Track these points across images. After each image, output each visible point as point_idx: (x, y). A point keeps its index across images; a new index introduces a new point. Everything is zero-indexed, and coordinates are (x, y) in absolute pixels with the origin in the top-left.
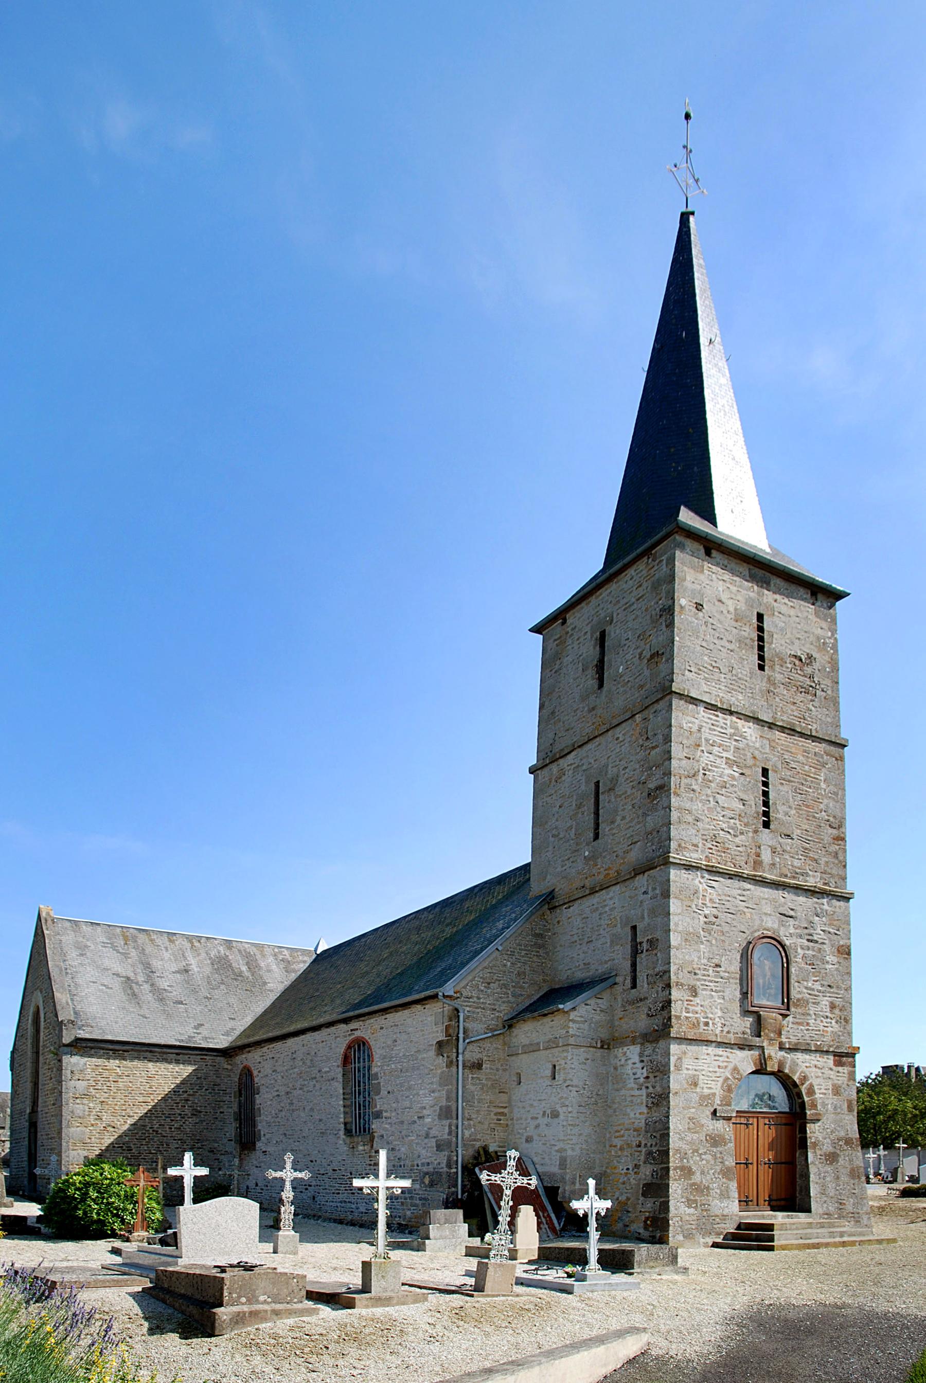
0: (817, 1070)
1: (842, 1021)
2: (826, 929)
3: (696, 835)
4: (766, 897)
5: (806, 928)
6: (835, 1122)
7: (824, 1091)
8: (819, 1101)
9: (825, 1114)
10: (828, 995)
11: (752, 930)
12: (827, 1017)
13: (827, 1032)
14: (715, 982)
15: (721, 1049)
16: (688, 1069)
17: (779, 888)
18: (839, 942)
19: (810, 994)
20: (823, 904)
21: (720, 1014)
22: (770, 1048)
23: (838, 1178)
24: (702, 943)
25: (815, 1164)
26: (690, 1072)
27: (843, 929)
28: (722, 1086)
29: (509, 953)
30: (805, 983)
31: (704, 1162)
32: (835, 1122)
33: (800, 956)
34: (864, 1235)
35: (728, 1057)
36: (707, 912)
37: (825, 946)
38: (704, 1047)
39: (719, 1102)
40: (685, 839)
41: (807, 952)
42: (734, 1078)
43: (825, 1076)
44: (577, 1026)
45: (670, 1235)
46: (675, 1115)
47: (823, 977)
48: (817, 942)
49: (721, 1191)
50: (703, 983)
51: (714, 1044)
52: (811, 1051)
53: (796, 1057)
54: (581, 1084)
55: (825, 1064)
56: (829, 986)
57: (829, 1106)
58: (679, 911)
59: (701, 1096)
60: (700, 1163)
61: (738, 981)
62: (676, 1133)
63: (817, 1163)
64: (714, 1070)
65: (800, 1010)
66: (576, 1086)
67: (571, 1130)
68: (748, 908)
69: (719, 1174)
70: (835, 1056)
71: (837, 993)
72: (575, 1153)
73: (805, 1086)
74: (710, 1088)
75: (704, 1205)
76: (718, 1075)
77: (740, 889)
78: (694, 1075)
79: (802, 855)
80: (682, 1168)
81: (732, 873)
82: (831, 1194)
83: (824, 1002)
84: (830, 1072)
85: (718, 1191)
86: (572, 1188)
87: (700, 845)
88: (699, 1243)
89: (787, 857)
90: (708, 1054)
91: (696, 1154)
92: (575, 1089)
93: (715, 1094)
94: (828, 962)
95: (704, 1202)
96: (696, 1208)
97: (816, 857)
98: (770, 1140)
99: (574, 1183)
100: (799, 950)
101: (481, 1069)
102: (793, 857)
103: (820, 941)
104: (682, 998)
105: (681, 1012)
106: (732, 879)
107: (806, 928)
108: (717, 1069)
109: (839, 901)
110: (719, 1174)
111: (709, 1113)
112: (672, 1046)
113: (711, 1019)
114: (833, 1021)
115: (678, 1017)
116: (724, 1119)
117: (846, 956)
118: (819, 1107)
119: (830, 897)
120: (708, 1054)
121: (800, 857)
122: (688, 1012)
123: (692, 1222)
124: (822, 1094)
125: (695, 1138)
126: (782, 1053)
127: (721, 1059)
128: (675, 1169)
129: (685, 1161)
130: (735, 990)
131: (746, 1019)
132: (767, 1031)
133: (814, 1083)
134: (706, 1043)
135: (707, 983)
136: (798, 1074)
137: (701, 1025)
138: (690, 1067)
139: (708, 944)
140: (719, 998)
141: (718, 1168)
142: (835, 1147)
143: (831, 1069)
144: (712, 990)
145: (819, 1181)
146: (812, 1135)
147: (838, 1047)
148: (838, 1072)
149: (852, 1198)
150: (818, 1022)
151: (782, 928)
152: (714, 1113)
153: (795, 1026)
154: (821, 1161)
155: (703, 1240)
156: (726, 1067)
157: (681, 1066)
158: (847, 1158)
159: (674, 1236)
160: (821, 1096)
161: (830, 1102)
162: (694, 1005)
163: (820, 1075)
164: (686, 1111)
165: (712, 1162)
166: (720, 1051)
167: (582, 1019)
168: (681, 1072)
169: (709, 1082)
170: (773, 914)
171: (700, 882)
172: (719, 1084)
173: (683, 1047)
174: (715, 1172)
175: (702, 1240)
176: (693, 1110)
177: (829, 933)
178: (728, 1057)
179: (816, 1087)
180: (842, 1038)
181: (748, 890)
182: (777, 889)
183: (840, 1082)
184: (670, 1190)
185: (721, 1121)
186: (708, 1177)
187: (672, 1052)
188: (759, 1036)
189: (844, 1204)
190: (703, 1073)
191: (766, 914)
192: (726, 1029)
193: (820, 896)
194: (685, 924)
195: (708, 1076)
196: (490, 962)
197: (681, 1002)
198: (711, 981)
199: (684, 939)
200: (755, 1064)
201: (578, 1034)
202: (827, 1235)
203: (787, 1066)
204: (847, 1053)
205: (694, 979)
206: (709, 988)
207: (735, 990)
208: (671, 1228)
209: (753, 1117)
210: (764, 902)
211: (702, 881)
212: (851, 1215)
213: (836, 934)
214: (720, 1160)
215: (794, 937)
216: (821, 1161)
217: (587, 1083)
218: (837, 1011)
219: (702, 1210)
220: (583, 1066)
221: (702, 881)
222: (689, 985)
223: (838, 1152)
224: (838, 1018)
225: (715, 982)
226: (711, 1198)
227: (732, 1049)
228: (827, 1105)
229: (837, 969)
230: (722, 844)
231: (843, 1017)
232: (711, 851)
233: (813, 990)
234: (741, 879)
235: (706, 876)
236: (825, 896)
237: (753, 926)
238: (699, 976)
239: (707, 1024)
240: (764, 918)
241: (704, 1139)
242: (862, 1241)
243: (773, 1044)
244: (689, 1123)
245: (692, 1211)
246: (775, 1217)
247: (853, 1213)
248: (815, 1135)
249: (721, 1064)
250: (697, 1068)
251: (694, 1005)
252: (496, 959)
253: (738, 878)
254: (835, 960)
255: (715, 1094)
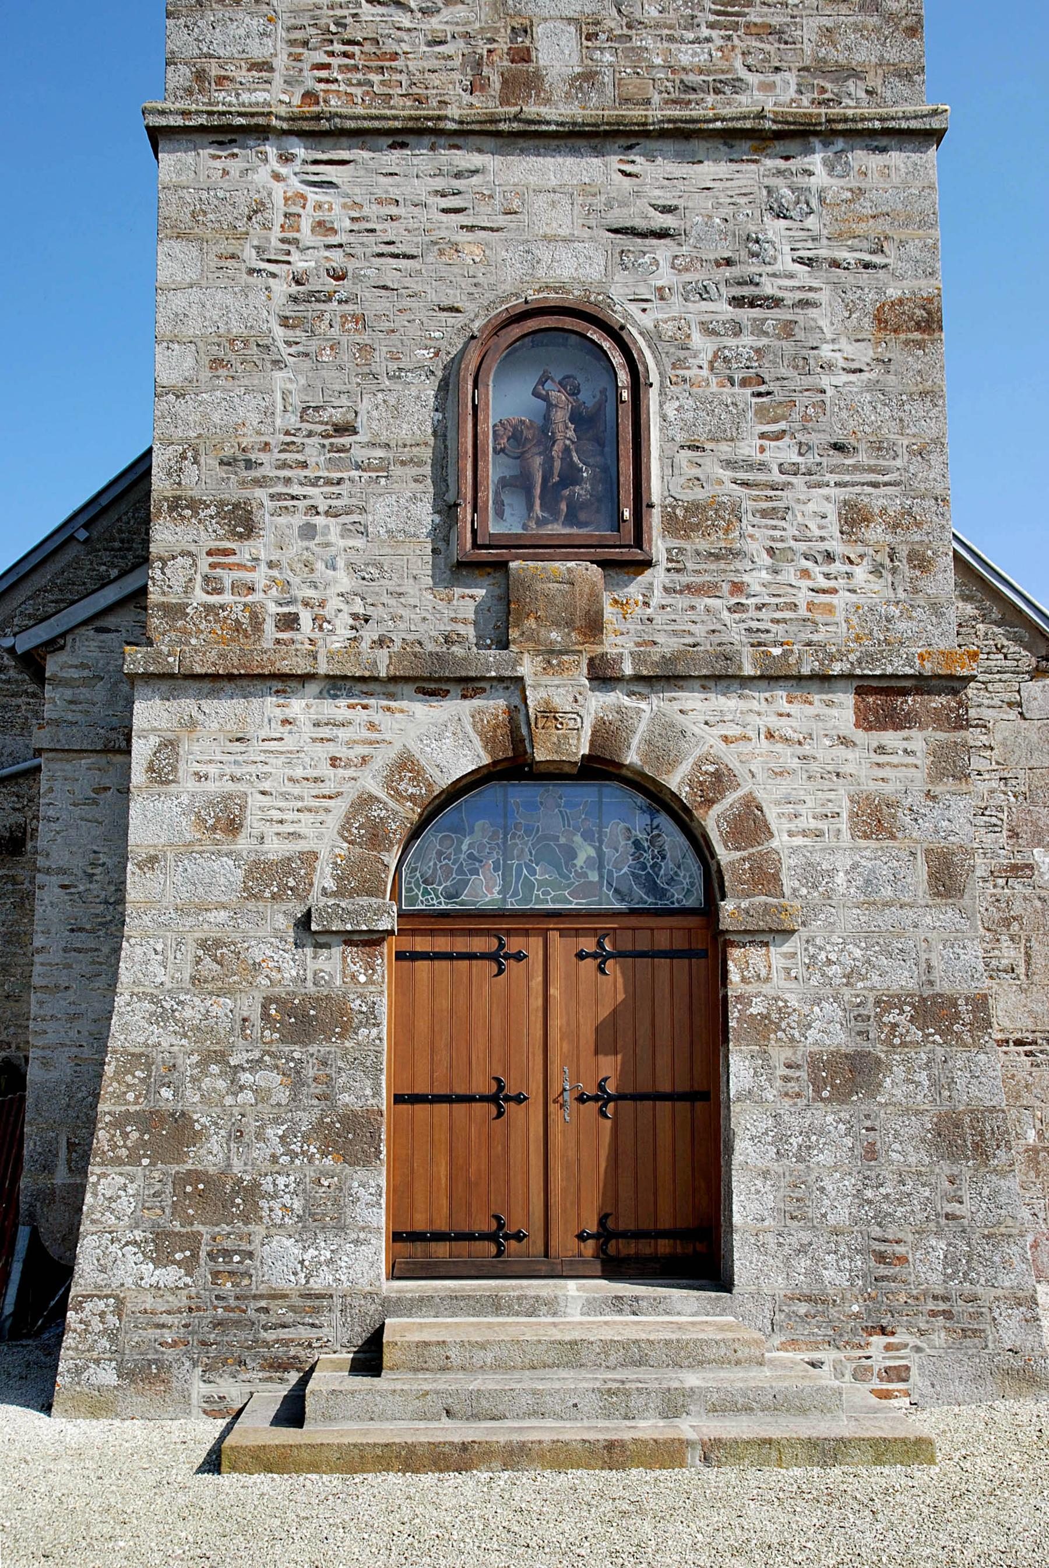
0: (779, 747)
1: (904, 566)
2: (823, 253)
3: (264, 34)
4: (554, 182)
5: (729, 262)
6: (867, 936)
7: (813, 824)
8: (788, 862)
9: (815, 910)
10: (832, 478)
11: (490, 296)
12: (829, 557)
13: (830, 609)
14: (329, 482)
15: (343, 702)
16: (199, 777)
17: (608, 145)
18: (880, 291)
19: (745, 484)
20: (811, 174)
21: (344, 581)
22: (546, 680)
23: (871, 1153)
24: (278, 364)
25: (762, 1101)
26: (211, 787)
27: (902, 243)
28: (345, 827)
29: (117, 545)
30: (724, 447)
31: (247, 1097)
32: (867, 936)
33: (704, 359)
34: (803, 1411)
35: (372, 726)
36: (300, 263)
37: (812, 312)
38: (271, 700)
39: (330, 885)
40: (221, 52)
41: (731, 342)
42: (398, 796)
43: (814, 767)
44: (68, 693)
45: (62, 1366)
46: (146, 936)
47: (806, 418)
48: (777, 302)
49: (310, 1203)
50: (280, 489)
51: (313, 688)
52: (746, 681)
53: (676, 706)
54: (78, 863)
55: (817, 727)
56: (838, 447)
57: (840, 878)
58: (193, 275)
59: (256, 863)
60: (229, 1100)
61: (427, 470)
62: (141, 997)
63: (770, 1095)
64: (315, 773)
65: (702, 544)
66: (62, 871)
67: (41, 1003)
68: (471, 228)
69: (306, 1139)
70: (860, 691)
71: (872, 470)
72: (54, 1075)
73: (717, 809)
74: (295, 835)
75: (227, 1253)
76: (327, 789)
77: (440, 173)
78: (230, 796)
79: (711, 26)
80: (148, 1120)
81: (398, 124)
82: (832, 1220)
83: (811, 507)
84: (841, 751)
85: (297, 1205)
86: (43, 1180)
87: (281, 62)
88: (186, 1398)
89: (649, 43)
90: (286, 722)
91: (214, 1069)
92: (55, 880)
93: (315, 855)
94: (827, 367)
95: (228, 1244)
96: (189, 1265)
97: (775, 21)
98: (605, 1012)
99: (48, 1168)
100: (697, 340)
101: (21, 854)
102: (671, 39)
103: (790, 297)
104: (192, 548)
105: (188, 590)
106: (403, 145)
107: (729, 262)
108: (325, 770)
109: (883, 150)
110: (306, 1139)
111: (284, 923)
112: (138, 706)
113: (306, 604)
114: (861, 573)
115: (175, 611)
116: (348, 943)
117: (917, 336)
118: (788, 883)
119: (840, 144)
120: (286, 722)
121: (705, 32)
122: (219, 591)
123: (165, 1319)
124: (804, 833)
125: (215, 1010)
126: (617, 698)
127: (342, 734)
128: (120, 1122)
129: (166, 1093)
130: (414, 499)
131: (458, 591)
132: (531, 623)
133: (761, 795)
134: (278, 685)
135: (296, 490)
136: (685, 768)
137: (269, 626)
138: (212, 770)
139: (306, 364)
140: (345, 532)
141: (306, 1119)
142: (864, 1034)
143: (845, 741)
144: (314, 510)
145: (775, 1167)
146: (750, 989)
147: (870, 658)
148: (881, 750)
149: (939, 1234)
150: (789, 575)
151: (620, 276)
152: (304, 923)
153: (681, 601)
154: (793, 1087)
155: (205, 1389)
156: (364, 761)
157: (175, 769)
158: (922, 1077)
159: (78, 1371)
160: (799, 841)
161: (843, 862)
162: (241, 566)
163: (795, 763)
164: (190, 921)
165: (283, 1096)
166: (339, 708)
167: (86, 673)
168: (172, 788)
169: (289, 816)
170: (586, 233)
171: (277, 177)
172: (333, 822)
173: (187, 705)
174: (292, 1132)
175: (199, 1389)
176: (222, 916)
177: (835, 264)
178: (372, 726)
179: (771, 814)
180: (902, 626)
181: (475, 172)
182: (599, 153)
183: (888, 789)
184: (89, 1199)
185: (337, 951)
186: (260, 1152)
187: (138, 722)
188: (504, 644)
189: (903, 1260)
190: (266, 786)
191: (547, 239)
192: (371, 634)
193: (792, 146)
194: (215, 314)
195: (285, 796)
196: (56, 575)
197: (188, 561)
198: (314, 482)
199: (205, 361)
200: (489, 743)
201: (70, 717)
202: (590, 1403)
203: (635, 742)
204: (919, 677)
205: (243, 483)
206: (301, 504)
207: (414, 499)
208: (69, 1340)
209: (526, 933)
210: (541, 201)
211: (283, 171)
212: (931, 1305)
213: (867, 266)
214: (317, 1089)
215: (676, 300)
216: (793, 1087)
217: (103, 859)
218: (876, 533)
219: (216, 1274)
220: (87, 811)
221: (283, 171)
222: (222, 504)
223: (880, 1051)
224: (883, 558)
225: (329, 482)
226: (259, 1230)
227: (391, 696)
228: (831, 873)
229: (870, 387)
230: (368, 47)
231: (903, 551)
232: (323, 74)
233: (762, 466)
234: (442, 141)
235: (300, 151)
236: (816, 143)
237: (492, 287)
238: (268, 471)
239: (289, 622)
240: (544, 253)
241: (256, 1014)
242: (718, 1443)
243: (562, 668)
244: (198, 961)
245: (170, 1275)
246: (552, 1305)
247: (945, 1299)
248: (766, 989)
249: (342, 752)
250: (238, 772)
251: (241, 566)
252: (75, 564)
253: (427, 140)
254: (864, 354)
255: (315, 855)
